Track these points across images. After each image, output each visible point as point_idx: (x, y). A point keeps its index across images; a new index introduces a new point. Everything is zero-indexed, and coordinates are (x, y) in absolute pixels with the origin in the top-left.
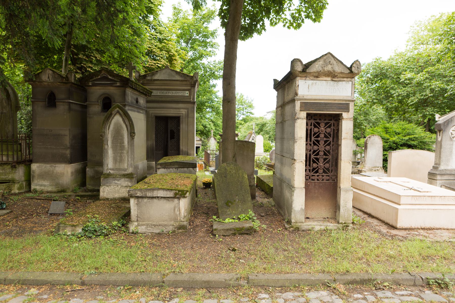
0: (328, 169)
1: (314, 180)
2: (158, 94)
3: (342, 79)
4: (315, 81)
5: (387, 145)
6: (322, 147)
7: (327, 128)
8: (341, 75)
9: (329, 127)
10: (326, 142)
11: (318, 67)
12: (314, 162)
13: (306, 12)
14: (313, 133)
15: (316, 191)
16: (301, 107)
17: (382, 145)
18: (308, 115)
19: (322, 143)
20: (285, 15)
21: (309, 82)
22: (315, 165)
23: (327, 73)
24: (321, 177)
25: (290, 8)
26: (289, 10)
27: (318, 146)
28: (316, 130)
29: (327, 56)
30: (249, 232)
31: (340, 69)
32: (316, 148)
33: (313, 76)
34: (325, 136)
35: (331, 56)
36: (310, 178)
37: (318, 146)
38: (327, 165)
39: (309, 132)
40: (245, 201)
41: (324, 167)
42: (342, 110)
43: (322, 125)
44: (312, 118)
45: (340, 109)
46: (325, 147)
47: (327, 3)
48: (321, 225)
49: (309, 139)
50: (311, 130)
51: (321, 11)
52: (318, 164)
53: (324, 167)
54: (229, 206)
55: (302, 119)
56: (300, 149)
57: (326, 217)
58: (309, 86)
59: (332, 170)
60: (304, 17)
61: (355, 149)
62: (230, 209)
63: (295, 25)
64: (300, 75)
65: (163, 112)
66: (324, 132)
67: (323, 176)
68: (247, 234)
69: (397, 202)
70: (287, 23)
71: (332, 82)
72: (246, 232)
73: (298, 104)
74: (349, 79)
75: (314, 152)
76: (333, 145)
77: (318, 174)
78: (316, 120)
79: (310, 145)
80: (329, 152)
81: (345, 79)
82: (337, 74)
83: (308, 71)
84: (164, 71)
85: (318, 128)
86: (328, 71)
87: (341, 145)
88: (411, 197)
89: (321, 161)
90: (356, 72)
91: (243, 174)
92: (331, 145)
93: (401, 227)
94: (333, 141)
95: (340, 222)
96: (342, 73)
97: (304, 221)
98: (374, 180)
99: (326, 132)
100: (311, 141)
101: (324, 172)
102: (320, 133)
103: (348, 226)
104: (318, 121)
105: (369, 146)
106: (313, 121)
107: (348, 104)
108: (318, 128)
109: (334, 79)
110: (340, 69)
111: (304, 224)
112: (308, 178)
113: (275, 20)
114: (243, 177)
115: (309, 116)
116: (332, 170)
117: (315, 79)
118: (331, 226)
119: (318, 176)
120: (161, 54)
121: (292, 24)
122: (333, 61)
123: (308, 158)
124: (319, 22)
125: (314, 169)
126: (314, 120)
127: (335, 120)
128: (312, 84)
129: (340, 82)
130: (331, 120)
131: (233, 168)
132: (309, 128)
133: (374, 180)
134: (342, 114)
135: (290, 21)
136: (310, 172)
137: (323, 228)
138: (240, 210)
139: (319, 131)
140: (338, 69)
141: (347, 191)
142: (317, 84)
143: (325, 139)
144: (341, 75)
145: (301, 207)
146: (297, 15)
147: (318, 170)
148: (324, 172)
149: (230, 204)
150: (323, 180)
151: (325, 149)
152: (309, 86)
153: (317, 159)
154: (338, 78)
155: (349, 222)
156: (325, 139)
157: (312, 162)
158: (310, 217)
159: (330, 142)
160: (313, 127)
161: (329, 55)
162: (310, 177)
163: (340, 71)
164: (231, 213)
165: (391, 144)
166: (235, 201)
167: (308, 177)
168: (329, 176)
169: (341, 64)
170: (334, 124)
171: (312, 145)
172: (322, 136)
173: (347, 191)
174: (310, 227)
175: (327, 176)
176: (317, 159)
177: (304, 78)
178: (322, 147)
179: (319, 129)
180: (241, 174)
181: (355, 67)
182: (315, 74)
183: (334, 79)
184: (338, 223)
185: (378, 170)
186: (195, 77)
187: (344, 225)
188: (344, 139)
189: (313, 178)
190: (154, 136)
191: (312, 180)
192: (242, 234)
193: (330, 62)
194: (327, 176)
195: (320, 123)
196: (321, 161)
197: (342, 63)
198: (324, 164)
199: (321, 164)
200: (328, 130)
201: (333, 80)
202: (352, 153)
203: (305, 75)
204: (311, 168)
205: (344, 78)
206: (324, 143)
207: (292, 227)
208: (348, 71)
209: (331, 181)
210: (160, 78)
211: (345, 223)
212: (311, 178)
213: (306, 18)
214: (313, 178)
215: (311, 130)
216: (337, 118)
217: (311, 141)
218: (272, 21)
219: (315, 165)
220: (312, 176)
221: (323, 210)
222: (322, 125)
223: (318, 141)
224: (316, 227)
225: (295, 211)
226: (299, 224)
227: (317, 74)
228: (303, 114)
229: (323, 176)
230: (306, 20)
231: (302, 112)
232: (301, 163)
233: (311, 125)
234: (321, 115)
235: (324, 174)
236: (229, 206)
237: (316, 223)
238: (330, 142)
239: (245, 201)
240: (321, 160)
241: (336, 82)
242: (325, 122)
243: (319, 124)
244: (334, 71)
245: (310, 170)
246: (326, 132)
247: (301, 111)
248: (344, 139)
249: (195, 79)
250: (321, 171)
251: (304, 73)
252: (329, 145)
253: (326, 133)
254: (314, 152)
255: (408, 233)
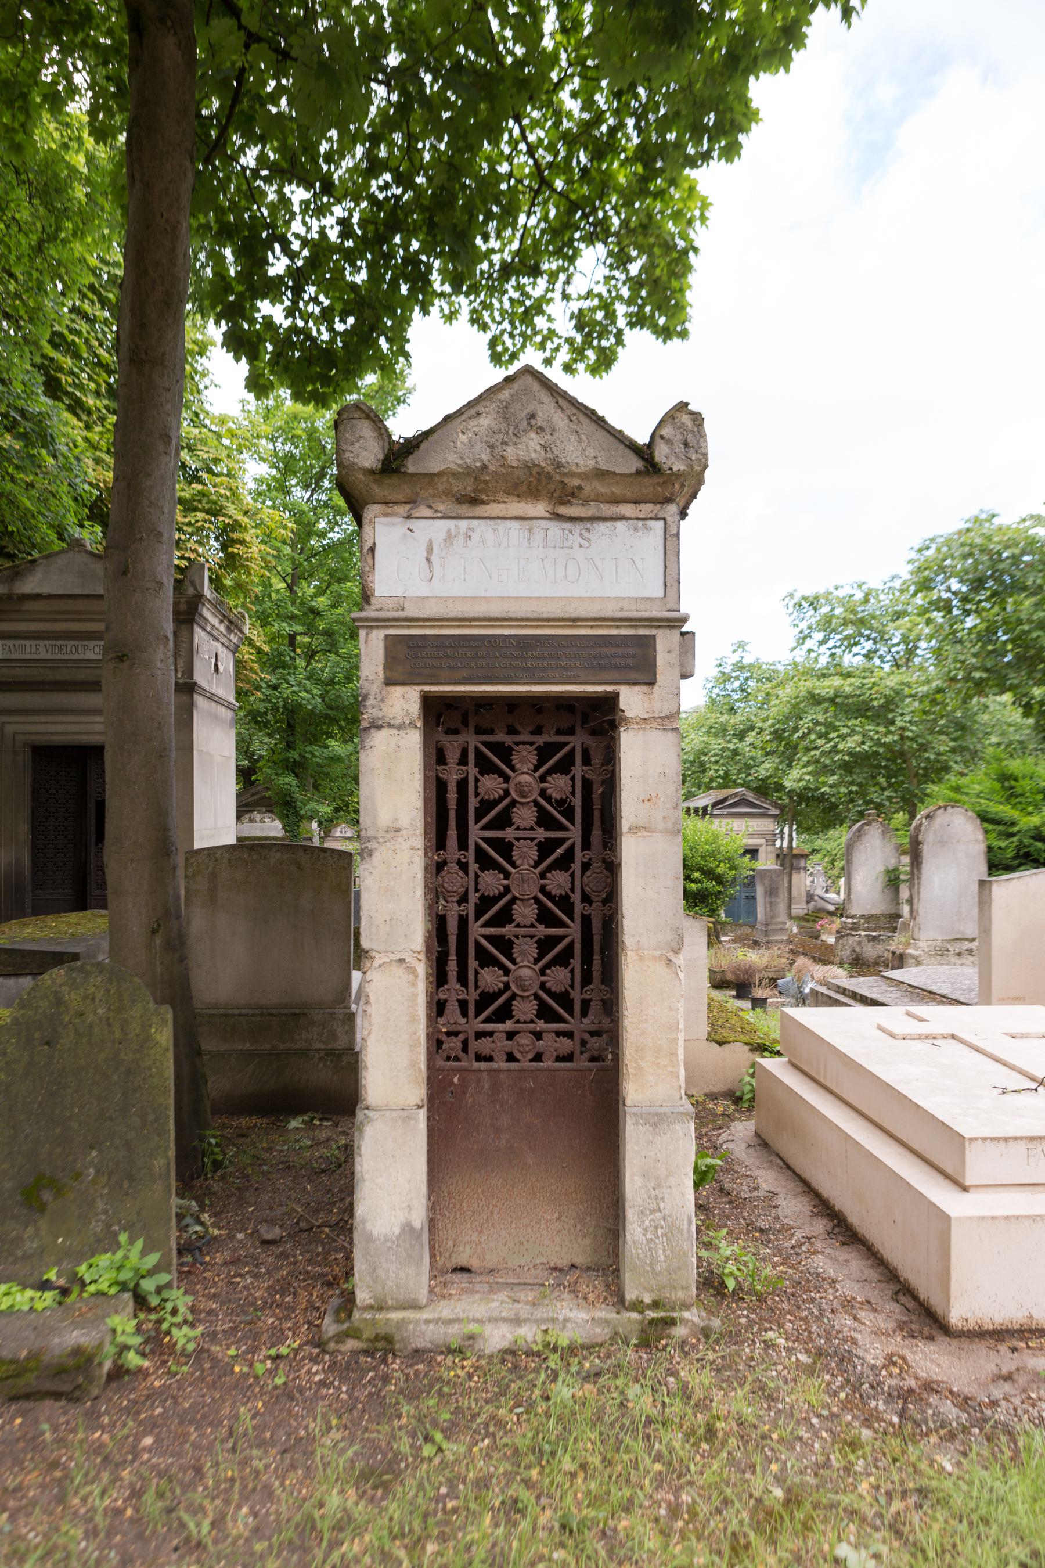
0: (564, 999)
1: (490, 1059)
2: (43, 655)
3: (607, 510)
4: (463, 524)
5: (1008, 847)
6: (525, 877)
7: (550, 772)
8: (602, 488)
9: (564, 767)
10: (545, 848)
11: (471, 443)
12: (486, 960)
13: (629, 302)
14: (473, 803)
15: (505, 1121)
16: (391, 660)
17: (982, 847)
18: (428, 703)
19: (526, 854)
20: (550, 319)
21: (432, 529)
22: (491, 978)
23: (520, 473)
24: (525, 1040)
25: (570, 290)
26: (566, 297)
27: (507, 875)
28: (491, 785)
29: (516, 386)
30: (67, 1388)
31: (590, 452)
32: (492, 882)
33: (448, 493)
34: (545, 820)
35: (536, 386)
36: (465, 1050)
37: (507, 875)
38: (558, 978)
39: (452, 796)
40: (131, 1178)
41: (543, 986)
42: (615, 675)
43: (525, 759)
44: (465, 723)
45: (602, 667)
46: (543, 876)
47: (696, 250)
48: (517, 1321)
49: (452, 833)
50: (462, 784)
51: (675, 284)
52: (507, 972)
53: (543, 986)
54: (42, 1208)
55: (400, 727)
56: (394, 896)
57: (564, 1262)
58: (430, 550)
59: (586, 1004)
60: (621, 322)
61: (892, 863)
62: (43, 1223)
63: (591, 354)
64: (377, 491)
65: (60, 728)
66: (535, 795)
67: (538, 1035)
68: (57, 1396)
69: (950, 1170)
70: (557, 349)
71: (555, 529)
72: (48, 1386)
73: (372, 653)
74: (647, 509)
75: (485, 902)
76: (586, 866)
77: (509, 1025)
78: (491, 732)
79: (463, 867)
80: (564, 902)
81: (627, 509)
82: (576, 482)
83: (412, 466)
84: (61, 561)
85: (501, 774)
86: (529, 467)
87: (620, 864)
88: (1022, 1146)
89: (522, 953)
90: (678, 466)
91: (146, 1026)
92: (576, 867)
93: (972, 1325)
94: (586, 846)
95: (630, 1296)
96: (600, 474)
97: (423, 1296)
98: (880, 1028)
99: (543, 793)
100: (463, 845)
101: (545, 1013)
102: (514, 803)
103: (672, 1322)
104: (500, 737)
105: (926, 850)
106: (473, 741)
107: (649, 642)
108: (501, 774)
109: (563, 510)
110: (590, 452)
111: (425, 1315)
112: (447, 1050)
113: (509, 342)
114: (148, 1039)
115: (438, 713)
116: (586, 1004)
117: (464, 509)
118: (577, 1319)
119: (510, 1035)
120: (189, 524)
121: (579, 353)
122: (547, 410)
123: (453, 940)
124: (683, 335)
125: (485, 999)
126: (479, 731)
127: (593, 733)
128: (449, 538)
129: (602, 527)
130: (571, 732)
131: (99, 995)
132: (452, 777)
133: (880, 1028)
134: (617, 695)
135: (570, 341)
136: (464, 1014)
137: (529, 1334)
138: (97, 1227)
139: (507, 793)
140: (578, 453)
141: (658, 1120)
142: (476, 536)
143: (541, 834)
144: (602, 488)
145: (401, 1217)
146: (599, 315)
147: (508, 1003)
148: (545, 1013)
149: (47, 1196)
150: (538, 1057)
151: (543, 889)
152: (430, 550)
153: (505, 945)
154: (586, 502)
155: (681, 1294)
156: (541, 834)
157: (473, 964)
158: (475, 1263)
159: (572, 848)
160: (472, 770)
161: (529, 379)
162: (465, 1043)
163: (591, 463)
164: (42, 1250)
165: (1027, 841)
166: (78, 1176)
167: (453, 1044)
168: (569, 1035)
169: (593, 427)
170: (586, 752)
171: (473, 867)
172: (525, 816)
173: (658, 1120)
174: (453, 1334)
175: (558, 1034)
176: (505, 945)
177: (403, 510)
178: (525, 877)
179: (507, 779)
180: (135, 1027)
181: (669, 442)
182: (457, 486)
183: (563, 510)
184: (621, 1303)
185: (970, 952)
186: (193, 583)
187: (651, 1314)
188: (634, 830)
189: (484, 1046)
190: (24, 828)
191: (479, 1058)
192: (27, 1397)
193: (532, 416)
194: (558, 1034)
195: (510, 750)
196: (522, 953)
197: (599, 421)
198: (542, 972)
199: (525, 972)
200: (558, 785)
201: (558, 517)
202: (882, 879)
203: (407, 490)
204: (473, 996)
205: (616, 501)
206: (534, 855)
207: (353, 1333)
208: (635, 464)
209: (582, 1062)
210: (44, 590)
211: (656, 1305)
212: (474, 1045)
213: (631, 325)
214: (484, 1046)
215: (462, 784)
216: (601, 718)
217: (463, 845)
218: (499, 348)
219: (491, 978)
220: (479, 1035)
221: (534, 1228)
222: (525, 759)
223: (505, 848)
224: (488, 1330)
225: (369, 1238)
226: (395, 1316)
227: (468, 487)
228: (405, 702)
229: (538, 1035)
230: (631, 336)
231: (398, 691)
232: (399, 971)
233: (463, 761)
234: (512, 704)
235: (541, 1025)
236: (42, 1208)
237: (499, 1303)
238: (572, 848)
239: (131, 1178)
240: (526, 950)
241: (578, 528)
242: (540, 740)
243: (505, 752)
244: (559, 466)
245: (463, 1005)
246: (543, 793)
247: (389, 682)
248: (634, 830)
249: (191, 591)
250: (524, 1009)
251: (395, 480)
252: (564, 863)
253: (548, 799)
254: (485, 902)
255: (1008, 1362)
